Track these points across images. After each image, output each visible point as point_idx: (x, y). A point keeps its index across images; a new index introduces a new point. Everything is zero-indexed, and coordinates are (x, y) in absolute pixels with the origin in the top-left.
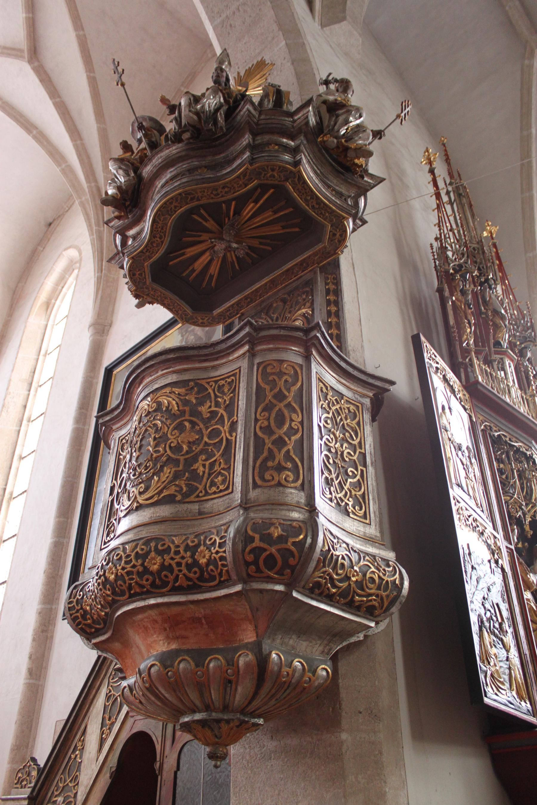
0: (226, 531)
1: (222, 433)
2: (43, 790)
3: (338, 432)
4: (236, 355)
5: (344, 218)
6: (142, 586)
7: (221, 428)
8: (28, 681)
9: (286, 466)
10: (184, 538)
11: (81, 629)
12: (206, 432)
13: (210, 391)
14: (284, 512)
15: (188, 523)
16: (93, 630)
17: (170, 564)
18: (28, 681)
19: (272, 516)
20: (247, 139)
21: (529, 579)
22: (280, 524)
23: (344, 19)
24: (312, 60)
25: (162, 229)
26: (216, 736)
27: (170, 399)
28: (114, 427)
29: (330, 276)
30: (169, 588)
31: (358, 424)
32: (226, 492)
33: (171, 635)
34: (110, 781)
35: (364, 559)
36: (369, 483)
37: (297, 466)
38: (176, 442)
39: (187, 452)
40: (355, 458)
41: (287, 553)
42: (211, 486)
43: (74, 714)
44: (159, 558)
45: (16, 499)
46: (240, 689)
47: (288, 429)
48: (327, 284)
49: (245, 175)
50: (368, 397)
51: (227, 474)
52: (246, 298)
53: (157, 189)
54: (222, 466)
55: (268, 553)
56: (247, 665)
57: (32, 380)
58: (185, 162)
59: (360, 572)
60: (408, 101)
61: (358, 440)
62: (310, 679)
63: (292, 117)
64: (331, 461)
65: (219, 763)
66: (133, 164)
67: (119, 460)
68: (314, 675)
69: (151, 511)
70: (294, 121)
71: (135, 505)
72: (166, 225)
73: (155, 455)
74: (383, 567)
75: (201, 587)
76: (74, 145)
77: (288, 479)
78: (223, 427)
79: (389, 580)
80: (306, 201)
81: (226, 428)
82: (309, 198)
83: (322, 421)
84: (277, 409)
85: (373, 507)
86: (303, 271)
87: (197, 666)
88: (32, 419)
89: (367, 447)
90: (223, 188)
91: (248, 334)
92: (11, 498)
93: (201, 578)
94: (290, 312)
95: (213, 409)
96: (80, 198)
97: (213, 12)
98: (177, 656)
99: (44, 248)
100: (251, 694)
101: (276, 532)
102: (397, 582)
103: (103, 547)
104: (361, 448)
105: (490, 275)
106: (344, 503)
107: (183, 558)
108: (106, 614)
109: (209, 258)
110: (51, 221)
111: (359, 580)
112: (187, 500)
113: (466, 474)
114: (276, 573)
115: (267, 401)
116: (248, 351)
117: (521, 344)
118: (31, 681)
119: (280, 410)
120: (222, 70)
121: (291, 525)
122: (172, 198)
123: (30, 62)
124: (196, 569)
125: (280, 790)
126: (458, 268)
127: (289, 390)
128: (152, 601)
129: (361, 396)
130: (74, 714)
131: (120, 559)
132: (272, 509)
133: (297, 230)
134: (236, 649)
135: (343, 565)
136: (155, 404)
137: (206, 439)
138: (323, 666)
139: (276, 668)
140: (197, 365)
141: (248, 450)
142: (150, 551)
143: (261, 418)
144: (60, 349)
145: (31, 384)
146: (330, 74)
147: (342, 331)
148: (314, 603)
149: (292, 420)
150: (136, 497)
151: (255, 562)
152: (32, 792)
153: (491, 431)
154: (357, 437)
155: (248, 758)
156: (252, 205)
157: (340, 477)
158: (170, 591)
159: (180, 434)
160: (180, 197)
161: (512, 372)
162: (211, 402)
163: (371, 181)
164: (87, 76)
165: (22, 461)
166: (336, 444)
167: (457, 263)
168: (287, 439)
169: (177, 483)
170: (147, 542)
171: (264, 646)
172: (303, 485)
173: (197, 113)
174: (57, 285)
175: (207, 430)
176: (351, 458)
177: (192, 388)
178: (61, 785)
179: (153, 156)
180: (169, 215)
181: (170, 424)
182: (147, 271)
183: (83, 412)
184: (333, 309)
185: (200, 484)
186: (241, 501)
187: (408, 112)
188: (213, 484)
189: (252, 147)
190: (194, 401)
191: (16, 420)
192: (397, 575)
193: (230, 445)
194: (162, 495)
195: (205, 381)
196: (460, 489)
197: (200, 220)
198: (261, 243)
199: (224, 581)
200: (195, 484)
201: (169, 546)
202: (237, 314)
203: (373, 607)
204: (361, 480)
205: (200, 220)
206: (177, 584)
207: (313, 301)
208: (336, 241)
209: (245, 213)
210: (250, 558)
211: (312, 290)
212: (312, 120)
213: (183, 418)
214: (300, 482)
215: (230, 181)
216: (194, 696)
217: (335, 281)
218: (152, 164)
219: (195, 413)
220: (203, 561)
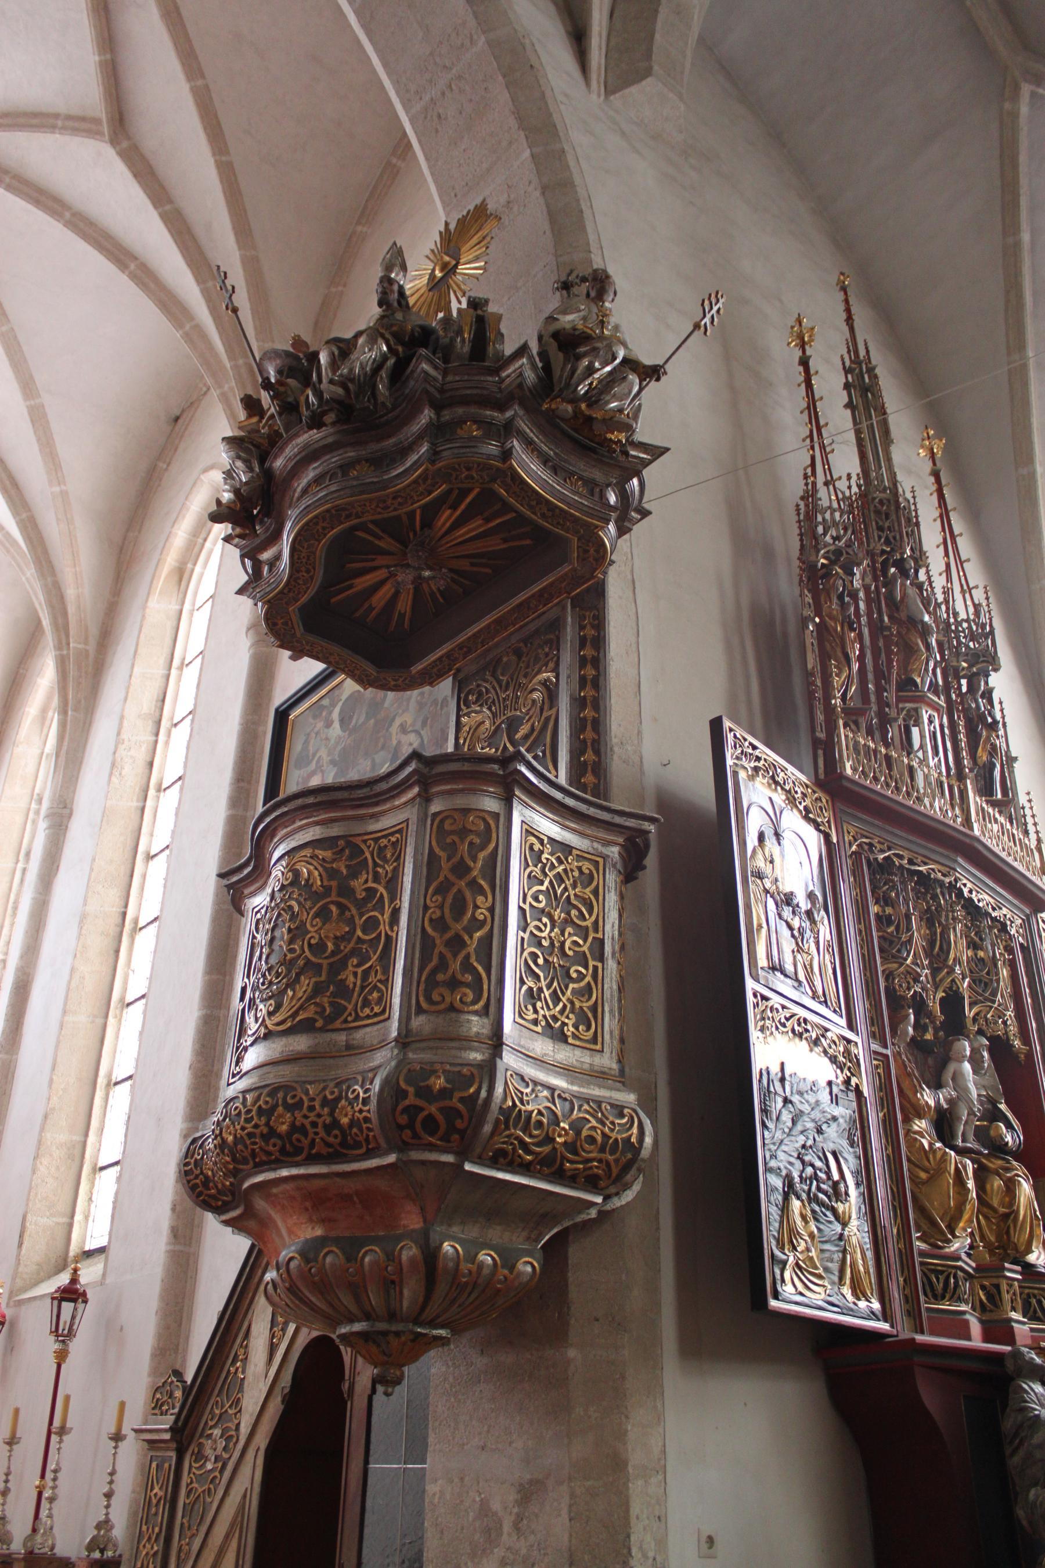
0: (371, 1083)
1: (379, 924)
2: (192, 1419)
3: (558, 910)
4: (404, 799)
5: (597, 527)
6: (269, 1153)
7: (380, 917)
8: (171, 1247)
9: (463, 980)
10: (322, 1085)
11: (204, 1201)
12: (359, 922)
13: (368, 855)
14: (454, 1052)
15: (332, 1061)
16: (220, 1203)
17: (303, 1125)
18: (171, 1247)
19: (435, 1058)
20: (426, 415)
21: (919, 1100)
22: (444, 1071)
23: (648, 72)
24: (577, 180)
25: (308, 559)
26: (385, 1354)
27: (311, 868)
28: (246, 891)
29: (587, 614)
30: (304, 1155)
31: (596, 892)
32: (382, 1018)
33: (314, 1218)
34: (282, 1407)
35: (579, 1110)
36: (606, 986)
37: (480, 979)
38: (317, 936)
39: (333, 953)
40: (585, 949)
41: (451, 1113)
42: (364, 1006)
43: (231, 1307)
44: (289, 1115)
45: (144, 930)
46: (406, 1292)
47: (469, 921)
48: (582, 628)
49: (425, 479)
50: (616, 844)
51: (384, 988)
52: (460, 647)
53: (296, 495)
54: (378, 977)
55: (425, 1113)
56: (412, 1260)
57: (161, 716)
58: (335, 453)
59: (570, 1129)
60: (717, 293)
61: (593, 918)
62: (505, 1278)
63: (498, 375)
64: (541, 961)
65: (390, 1390)
66: (257, 446)
67: (253, 944)
68: (511, 1273)
69: (282, 1043)
70: (502, 381)
71: (263, 1030)
72: (314, 553)
73: (289, 956)
74: (611, 1118)
75: (345, 1155)
76: (202, 291)
77: (464, 999)
78: (383, 915)
79: (619, 1137)
80: (531, 508)
81: (387, 916)
82: (534, 503)
83: (529, 899)
84: (455, 890)
85: (610, 1023)
86: (545, 605)
87: (349, 1259)
88: (164, 786)
89: (608, 927)
90: (394, 498)
91: (415, 772)
92: (137, 929)
93: (344, 1144)
94: (525, 676)
95: (370, 884)
96: (220, 387)
97: (408, 91)
98: (323, 1247)
99: (168, 465)
100: (421, 1299)
101: (439, 1082)
102: (633, 1139)
103: (231, 1081)
104: (596, 930)
105: (905, 552)
106: (559, 1023)
107: (319, 1116)
108: (232, 1184)
109: (393, 590)
110: (178, 414)
111: (569, 1140)
112: (330, 1027)
113: (797, 944)
114: (440, 1139)
115: (441, 878)
116: (419, 795)
117: (971, 666)
118: (178, 1248)
119: (459, 891)
120: (391, 281)
121: (459, 1072)
122: (316, 517)
123: (114, 142)
124: (336, 1132)
125: (490, 1426)
126: (833, 558)
127: (474, 859)
128: (285, 1173)
129: (603, 845)
130: (231, 1307)
131: (239, 1114)
132: (437, 1048)
133: (528, 542)
134: (399, 1238)
135: (540, 1124)
136: (290, 874)
137: (359, 933)
138: (527, 1259)
139: (451, 1264)
140: (350, 813)
141: (413, 954)
142: (276, 1105)
143: (433, 905)
144: (203, 659)
145: (158, 723)
146: (571, 272)
147: (602, 713)
148: (501, 1175)
149: (476, 907)
150: (264, 1020)
151: (411, 1125)
153: (872, 852)
154: (591, 913)
155: (451, 1379)
156: (448, 512)
157: (555, 984)
158: (306, 1159)
159: (324, 924)
160: (328, 515)
161: (934, 733)
162: (368, 873)
163: (645, 456)
164: (216, 161)
165: (151, 863)
166: (552, 930)
167: (832, 548)
168: (466, 938)
169: (318, 1000)
170: (274, 1091)
171: (432, 1235)
172: (487, 1006)
173: (343, 385)
174: (194, 536)
175: (360, 918)
176: (577, 949)
177: (343, 850)
178: (217, 1412)
179: (291, 439)
180: (317, 540)
181: (311, 908)
182: (296, 619)
183: (242, 788)
184: (590, 672)
185: (350, 1003)
186: (399, 1034)
187: (719, 310)
188: (366, 1003)
189: (438, 431)
190: (345, 872)
191: (137, 789)
192: (635, 1130)
193: (390, 943)
194: (298, 1019)
195: (360, 838)
196: (778, 974)
197: (371, 538)
198: (472, 564)
199: (373, 1149)
200: (342, 1002)
201: (301, 1099)
202: (450, 670)
203: (597, 1177)
204: (593, 983)
205: (371, 538)
206: (314, 1151)
207: (558, 658)
208: (591, 559)
209: (440, 523)
210: (403, 1119)
211: (558, 638)
212: (530, 376)
213: (329, 900)
214: (482, 1003)
215: (404, 488)
216: (347, 1300)
217: (596, 622)
218: (284, 455)
219: (346, 891)
220: (345, 1120)
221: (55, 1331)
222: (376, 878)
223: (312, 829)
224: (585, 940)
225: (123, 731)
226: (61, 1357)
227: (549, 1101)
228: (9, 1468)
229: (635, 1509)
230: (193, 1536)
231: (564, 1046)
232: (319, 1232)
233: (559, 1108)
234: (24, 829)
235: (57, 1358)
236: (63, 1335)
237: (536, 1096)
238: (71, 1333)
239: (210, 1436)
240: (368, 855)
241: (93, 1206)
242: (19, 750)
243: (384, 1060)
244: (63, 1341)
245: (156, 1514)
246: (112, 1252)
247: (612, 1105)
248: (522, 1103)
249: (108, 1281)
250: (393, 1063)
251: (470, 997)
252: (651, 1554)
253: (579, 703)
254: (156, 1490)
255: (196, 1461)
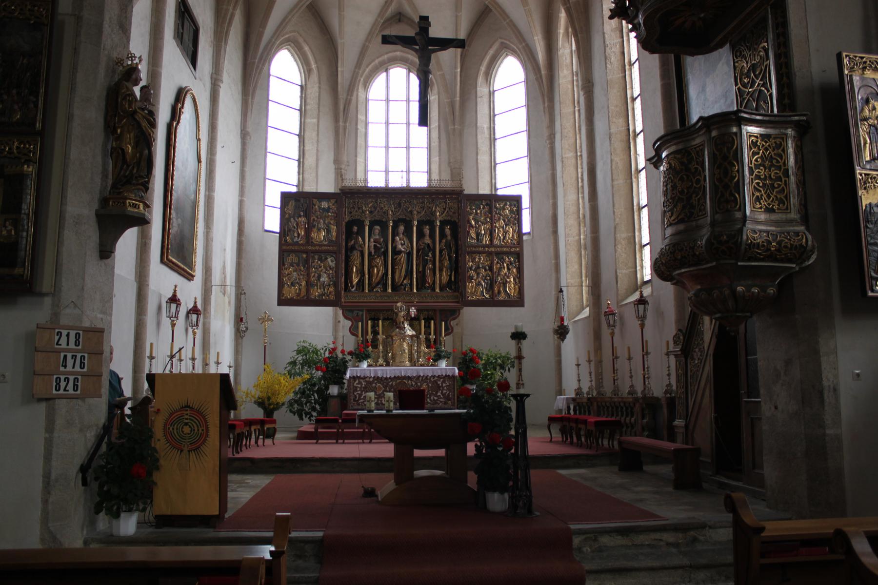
3: (767, 162)
7: (700, 178)
12: (694, 180)
35: (780, 237)
42: (699, 212)
59: (777, 244)
73: (673, 196)
79: (797, 244)
88: (632, 63)
94: (756, 44)
95: (696, 166)
106: (771, 206)
111: (777, 248)
135: (763, 246)
137: (695, 185)
148: (753, 264)
152: (682, 347)
154: (782, 159)
157: (768, 191)
166: (765, 171)
178: (696, 343)
188: (700, 210)
191: (620, 68)
192: (804, 240)
193: (705, 187)
194: (679, 218)
220: (697, 253)
221: (638, 317)
222: (697, 164)
223: (673, 146)
224: (780, 171)
225: (606, 40)
226: (642, 326)
227: (766, 237)
228: (630, 368)
229: (824, 366)
230: (694, 386)
231: (775, 214)
232: (699, 287)
233: (771, 238)
234: (574, 91)
235: (641, 326)
236: (642, 319)
237: (761, 236)
238: (645, 317)
239: (695, 351)
240: (693, 154)
241: (644, 262)
242: (560, 53)
243: (706, 233)
244: (642, 320)
245: (681, 379)
246: (654, 281)
247: (794, 233)
248: (754, 240)
249: (654, 294)
250: (709, 233)
251: (734, 205)
252: (831, 380)
253: (777, 57)
254: (680, 371)
255: (692, 360)
